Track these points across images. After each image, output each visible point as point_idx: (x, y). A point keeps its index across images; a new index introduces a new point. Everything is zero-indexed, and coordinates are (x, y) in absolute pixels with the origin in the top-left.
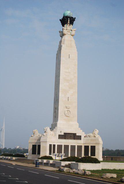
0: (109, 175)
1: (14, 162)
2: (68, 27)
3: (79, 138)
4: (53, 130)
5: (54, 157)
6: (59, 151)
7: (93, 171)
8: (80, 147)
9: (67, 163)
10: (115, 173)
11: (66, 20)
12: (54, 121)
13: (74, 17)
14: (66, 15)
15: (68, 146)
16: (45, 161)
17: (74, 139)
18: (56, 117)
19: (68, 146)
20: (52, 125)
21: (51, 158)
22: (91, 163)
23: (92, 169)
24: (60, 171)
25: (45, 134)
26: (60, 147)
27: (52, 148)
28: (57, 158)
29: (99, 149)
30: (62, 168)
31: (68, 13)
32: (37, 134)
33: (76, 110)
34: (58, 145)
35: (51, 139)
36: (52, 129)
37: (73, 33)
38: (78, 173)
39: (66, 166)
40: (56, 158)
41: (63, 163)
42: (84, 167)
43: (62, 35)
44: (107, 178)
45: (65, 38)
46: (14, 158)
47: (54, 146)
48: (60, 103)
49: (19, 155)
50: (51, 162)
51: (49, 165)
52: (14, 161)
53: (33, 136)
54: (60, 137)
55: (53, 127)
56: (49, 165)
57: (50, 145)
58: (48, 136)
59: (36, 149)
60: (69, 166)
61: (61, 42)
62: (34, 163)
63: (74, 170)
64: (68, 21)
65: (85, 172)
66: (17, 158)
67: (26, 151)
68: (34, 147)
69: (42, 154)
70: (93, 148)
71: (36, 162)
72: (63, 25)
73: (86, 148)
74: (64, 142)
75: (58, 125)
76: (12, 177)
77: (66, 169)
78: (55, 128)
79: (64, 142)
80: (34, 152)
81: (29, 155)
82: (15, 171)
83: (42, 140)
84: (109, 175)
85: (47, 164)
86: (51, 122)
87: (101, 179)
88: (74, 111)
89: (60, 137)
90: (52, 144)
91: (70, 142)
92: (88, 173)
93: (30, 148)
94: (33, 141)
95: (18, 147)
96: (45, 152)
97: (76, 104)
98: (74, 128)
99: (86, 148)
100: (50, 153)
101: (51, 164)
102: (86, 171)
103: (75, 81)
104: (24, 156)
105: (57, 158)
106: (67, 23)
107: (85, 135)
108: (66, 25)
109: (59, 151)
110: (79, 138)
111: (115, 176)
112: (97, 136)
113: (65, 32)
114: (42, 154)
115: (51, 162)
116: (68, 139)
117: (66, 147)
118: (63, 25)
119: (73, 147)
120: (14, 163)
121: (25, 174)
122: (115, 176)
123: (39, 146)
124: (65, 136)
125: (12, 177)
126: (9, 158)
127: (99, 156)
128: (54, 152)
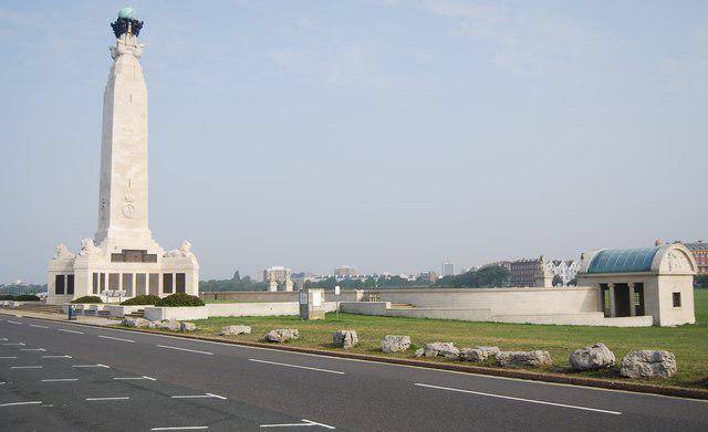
0: (236, 329)
1: (18, 312)
2: (127, 39)
3: (153, 258)
4: (99, 244)
5: (104, 298)
6: (114, 285)
7: (197, 322)
8: (154, 277)
9: (136, 308)
10: (246, 324)
11: (121, 27)
12: (100, 227)
13: (140, 21)
14: (124, 16)
15: (118, 275)
16: (87, 306)
17: (143, 261)
18: (104, 218)
19: (131, 275)
20: (97, 235)
21: (98, 300)
22: (249, 304)
23: (196, 318)
24: (126, 325)
25: (83, 253)
26: (114, 277)
27: (98, 280)
28: (110, 300)
29: (192, 279)
30: (130, 319)
31: (128, 12)
32: (66, 254)
33: (146, 203)
34: (110, 275)
35: (97, 261)
36: (97, 242)
37: (139, 51)
38: (166, 329)
39: (134, 315)
40: (108, 299)
41: (128, 310)
42: (174, 315)
43: (117, 55)
44: (232, 335)
45: (124, 61)
46: (17, 304)
47: (103, 275)
48: (112, 191)
49: (29, 297)
50: (100, 307)
51: (97, 314)
52: (16, 308)
53: (56, 257)
54: (115, 257)
55: (100, 238)
56: (97, 314)
57: (95, 275)
58: (90, 257)
59: (65, 284)
60: (141, 314)
61: (113, 69)
62: (62, 312)
63: (158, 322)
64: (127, 27)
65: (183, 326)
66: (22, 303)
67: (44, 289)
68: (60, 279)
69: (78, 294)
70: (181, 277)
71: (70, 310)
72: (118, 36)
73: (168, 277)
74: (122, 268)
75: (110, 235)
76: (43, 403)
77: (138, 322)
78: (102, 240)
79: (122, 268)
80: (59, 290)
81: (51, 297)
82: (25, 328)
83: (77, 264)
84: (236, 329)
85: (90, 313)
86: (95, 229)
87: (222, 338)
88: (142, 207)
89: (115, 257)
90: (99, 272)
91: (135, 268)
92: (191, 327)
93: (51, 283)
94: (58, 267)
95: (19, 282)
96: (84, 288)
97: (144, 194)
98: (142, 240)
99: (168, 277)
100: (95, 291)
101: (100, 312)
102: (186, 324)
103: (144, 149)
104: (38, 299)
105: (110, 300)
106: (125, 31)
107: (164, 253)
108: (123, 36)
109: (114, 285)
110: (153, 258)
111: (247, 329)
112: (189, 254)
113: (122, 48)
114: (78, 294)
115: (100, 307)
116: (130, 261)
117: (127, 277)
118: (118, 36)
119: (141, 278)
120: (19, 314)
121: (50, 334)
122: (247, 329)
123: (71, 278)
124: (125, 256)
125: (43, 403)
126: (6, 303)
127: (192, 289)
128: (103, 288)
